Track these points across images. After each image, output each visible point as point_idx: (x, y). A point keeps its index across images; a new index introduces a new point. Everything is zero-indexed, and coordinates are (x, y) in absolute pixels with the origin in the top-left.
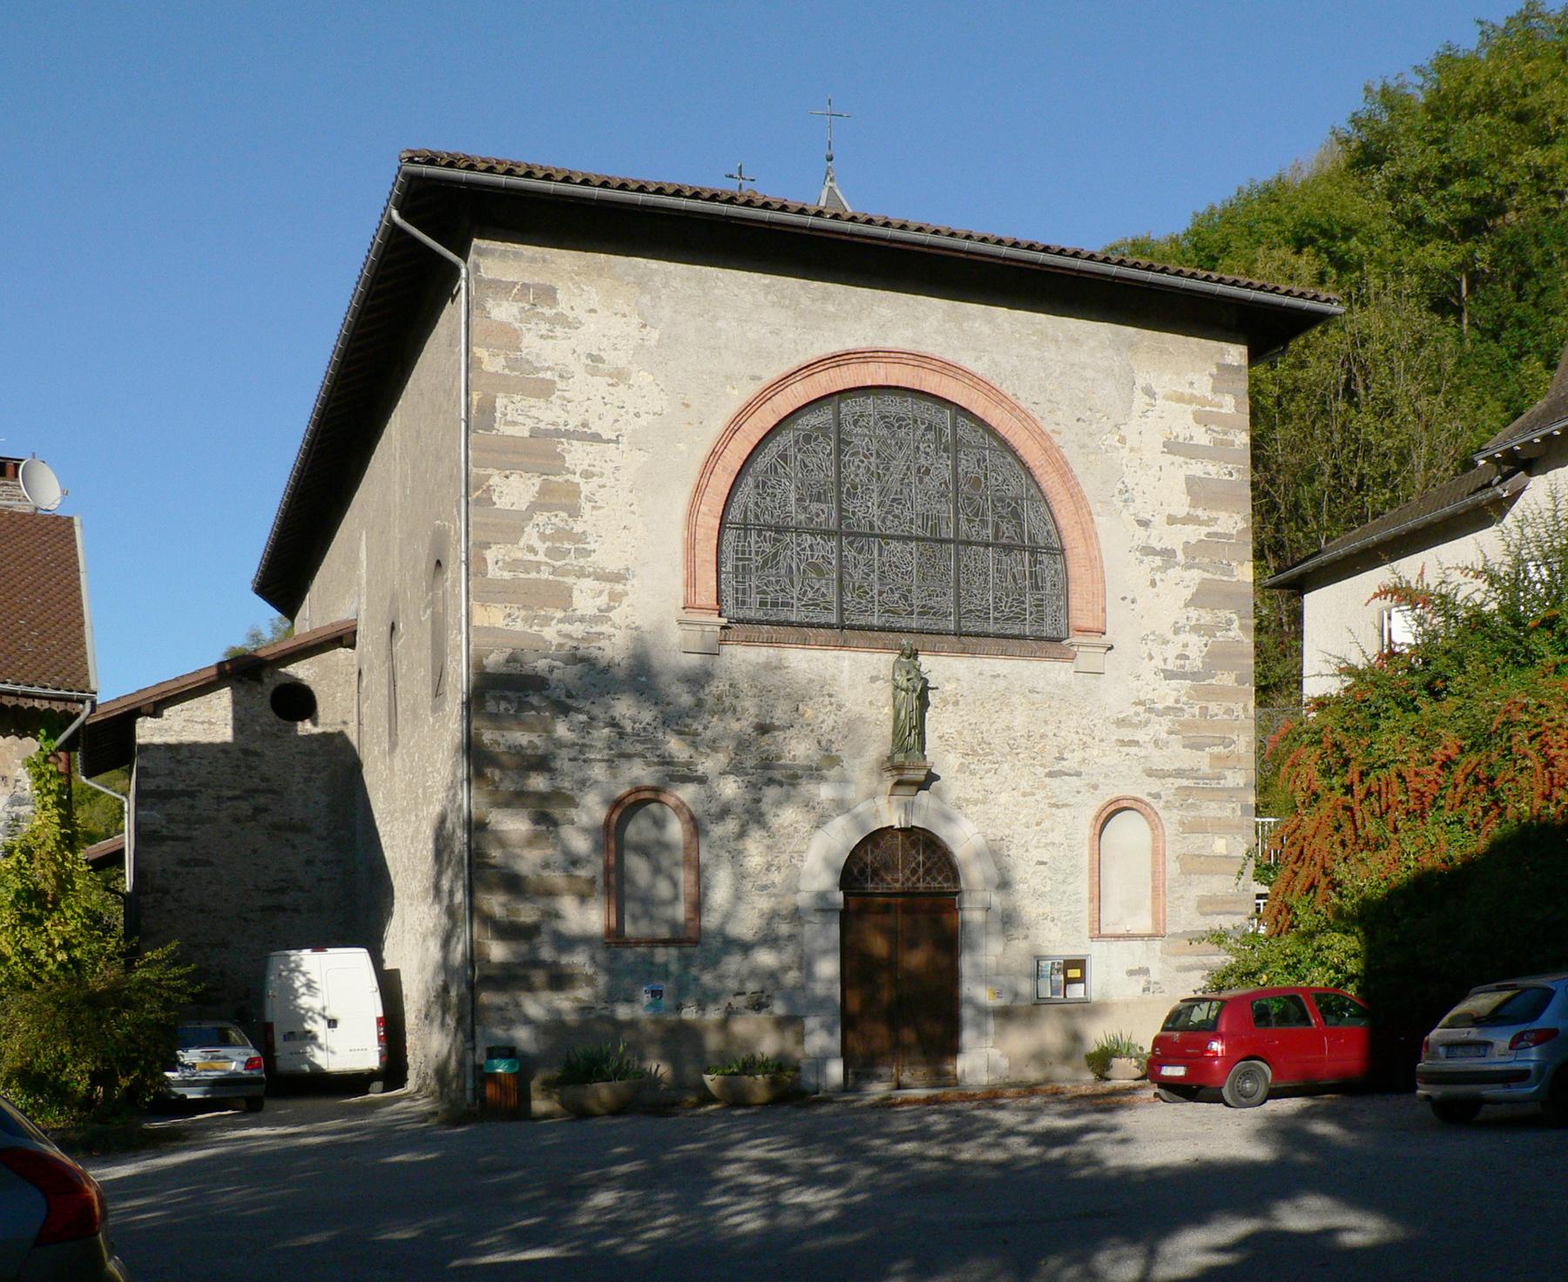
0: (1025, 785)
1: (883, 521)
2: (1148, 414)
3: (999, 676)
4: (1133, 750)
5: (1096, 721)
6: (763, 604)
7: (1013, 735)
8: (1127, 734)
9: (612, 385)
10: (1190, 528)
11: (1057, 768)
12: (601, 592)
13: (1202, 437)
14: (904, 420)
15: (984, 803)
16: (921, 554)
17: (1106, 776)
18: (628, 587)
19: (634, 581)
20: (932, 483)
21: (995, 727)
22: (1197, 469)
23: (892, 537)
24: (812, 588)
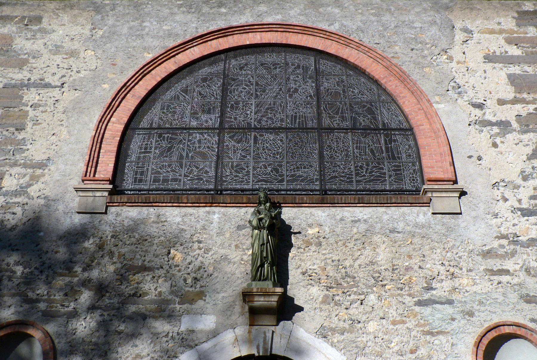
0: (393, 314)
2: (469, 42)
3: (359, 220)
4: (505, 279)
5: (460, 254)
7: (377, 268)
8: (495, 264)
9: (66, 58)
10: (518, 106)
11: (426, 296)
12: (25, 176)
13: (514, 51)
14: (278, 64)
15: (351, 331)
16: (290, 140)
17: (481, 303)
20: (300, 97)
21: (358, 262)
22: (515, 70)
24: (197, 168)
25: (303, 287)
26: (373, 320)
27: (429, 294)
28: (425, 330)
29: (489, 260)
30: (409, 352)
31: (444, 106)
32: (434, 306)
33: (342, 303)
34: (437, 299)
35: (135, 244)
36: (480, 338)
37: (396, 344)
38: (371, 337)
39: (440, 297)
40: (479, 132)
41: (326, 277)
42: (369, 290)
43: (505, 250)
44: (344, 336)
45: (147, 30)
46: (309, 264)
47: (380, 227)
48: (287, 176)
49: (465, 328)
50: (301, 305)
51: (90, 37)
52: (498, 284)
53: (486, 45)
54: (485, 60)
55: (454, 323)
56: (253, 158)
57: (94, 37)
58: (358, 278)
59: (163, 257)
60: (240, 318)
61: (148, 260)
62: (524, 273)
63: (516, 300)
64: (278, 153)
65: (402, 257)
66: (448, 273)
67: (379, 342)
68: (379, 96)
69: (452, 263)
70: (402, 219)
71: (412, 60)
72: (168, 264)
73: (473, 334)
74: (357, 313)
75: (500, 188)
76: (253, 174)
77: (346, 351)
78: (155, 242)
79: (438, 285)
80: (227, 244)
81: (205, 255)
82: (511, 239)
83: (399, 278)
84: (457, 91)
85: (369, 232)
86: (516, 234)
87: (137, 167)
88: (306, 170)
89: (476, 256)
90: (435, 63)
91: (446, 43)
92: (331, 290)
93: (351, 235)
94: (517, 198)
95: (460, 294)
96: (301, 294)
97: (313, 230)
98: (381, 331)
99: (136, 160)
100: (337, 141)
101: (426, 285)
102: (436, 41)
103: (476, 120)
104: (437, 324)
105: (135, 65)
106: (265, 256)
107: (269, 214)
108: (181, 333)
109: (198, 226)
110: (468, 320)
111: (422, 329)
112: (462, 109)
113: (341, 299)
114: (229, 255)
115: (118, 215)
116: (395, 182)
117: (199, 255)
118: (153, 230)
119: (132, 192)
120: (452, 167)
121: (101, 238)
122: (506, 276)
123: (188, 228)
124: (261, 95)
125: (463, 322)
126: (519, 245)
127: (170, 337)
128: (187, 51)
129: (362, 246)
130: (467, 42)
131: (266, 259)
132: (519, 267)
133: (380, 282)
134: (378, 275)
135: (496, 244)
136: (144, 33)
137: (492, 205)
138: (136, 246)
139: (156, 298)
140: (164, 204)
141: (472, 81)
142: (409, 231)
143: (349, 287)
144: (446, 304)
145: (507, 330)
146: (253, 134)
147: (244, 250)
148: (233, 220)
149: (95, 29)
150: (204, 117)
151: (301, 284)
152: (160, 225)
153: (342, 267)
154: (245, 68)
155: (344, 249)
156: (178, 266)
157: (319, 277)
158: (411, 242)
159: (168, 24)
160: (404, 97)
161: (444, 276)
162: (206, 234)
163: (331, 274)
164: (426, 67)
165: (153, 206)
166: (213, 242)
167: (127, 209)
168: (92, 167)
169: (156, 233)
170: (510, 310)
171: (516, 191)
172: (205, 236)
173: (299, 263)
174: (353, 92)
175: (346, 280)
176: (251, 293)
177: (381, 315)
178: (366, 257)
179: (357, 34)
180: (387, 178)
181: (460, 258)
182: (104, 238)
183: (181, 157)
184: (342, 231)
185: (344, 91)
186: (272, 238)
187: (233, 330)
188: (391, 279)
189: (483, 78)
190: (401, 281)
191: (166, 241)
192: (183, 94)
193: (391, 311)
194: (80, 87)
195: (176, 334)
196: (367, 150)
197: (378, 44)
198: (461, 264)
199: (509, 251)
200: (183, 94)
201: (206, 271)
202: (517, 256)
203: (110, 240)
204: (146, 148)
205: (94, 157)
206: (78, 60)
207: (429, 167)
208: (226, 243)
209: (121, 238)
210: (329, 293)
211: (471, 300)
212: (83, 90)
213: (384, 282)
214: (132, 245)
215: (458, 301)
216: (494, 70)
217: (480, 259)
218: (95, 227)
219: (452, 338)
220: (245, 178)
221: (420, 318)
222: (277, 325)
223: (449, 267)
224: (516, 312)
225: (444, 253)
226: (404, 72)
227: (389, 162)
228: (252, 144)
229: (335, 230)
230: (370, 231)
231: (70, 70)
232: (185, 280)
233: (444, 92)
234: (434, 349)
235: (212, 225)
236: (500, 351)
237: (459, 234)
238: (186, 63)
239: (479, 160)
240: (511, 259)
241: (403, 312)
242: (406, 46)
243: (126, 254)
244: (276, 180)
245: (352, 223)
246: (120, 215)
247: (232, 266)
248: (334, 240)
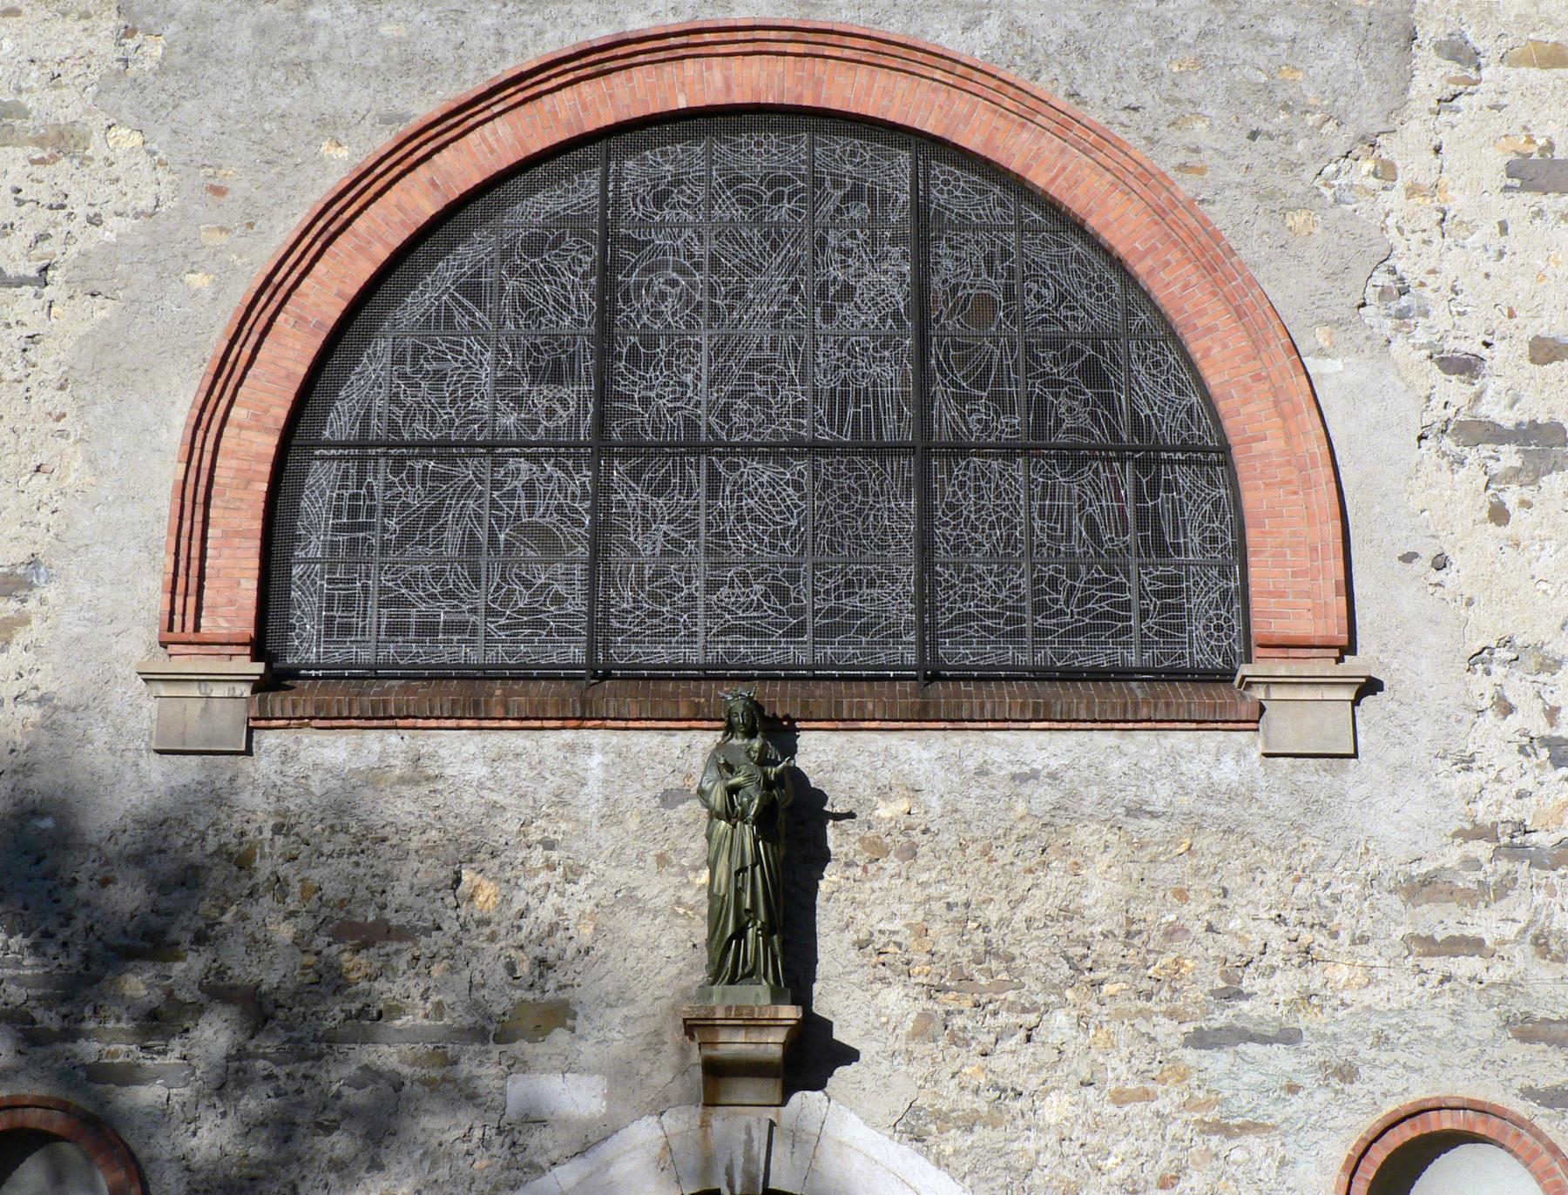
0: (1118, 1071)
1: (724, 415)
2: (1461, 102)
3: (1035, 775)
4: (1466, 966)
5: (1336, 889)
6: (395, 629)
7: (1080, 930)
8: (1441, 920)
9: (42, 161)
11: (1220, 1019)
14: (787, 181)
15: (993, 1122)
16: (827, 485)
17: (1382, 1040)
18: (32, 605)
19: (51, 592)
20: (858, 318)
21: (1025, 910)
23: (749, 450)
24: (528, 585)
25: (860, 987)
26: (1060, 1089)
27: (1229, 1012)
28: (1206, 1119)
29: (1425, 907)
30: (1155, 1184)
31: (1341, 368)
32: (1242, 1047)
33: (973, 1038)
34: (1250, 1027)
35: (350, 854)
36: (1364, 1145)
37: (1119, 1159)
38: (1051, 1139)
39: (1261, 1021)
40: (1452, 464)
41: (929, 956)
42: (1053, 998)
43: (1481, 876)
44: (974, 1137)
45: (322, 38)
46: (877, 916)
47: (1096, 798)
48: (815, 613)
49: (1324, 1114)
50: (852, 1045)
51: (119, 72)
52: (1441, 982)
53: (1524, 117)
54: (1509, 181)
55: (1293, 1100)
56: (708, 552)
57: (133, 68)
58: (1023, 960)
59: (441, 895)
60: (677, 1083)
61: (394, 906)
62: (1529, 949)
63: (1489, 1033)
64: (785, 531)
65: (1157, 896)
66: (1294, 947)
67: (1071, 1152)
68: (1129, 314)
69: (1308, 917)
70: (1166, 770)
71: (1249, 179)
72: (458, 917)
73: (1346, 1133)
74: (1015, 1066)
75: (1494, 667)
76: (708, 607)
77: (976, 1181)
78: (414, 845)
79: (1260, 984)
80: (631, 853)
81: (567, 886)
82: (1505, 840)
83: (1145, 960)
84: (1395, 306)
85: (1062, 814)
86: (1522, 823)
87: (330, 581)
88: (875, 592)
89: (1385, 894)
90: (1328, 193)
91: (1377, 106)
92: (940, 996)
93: (1008, 825)
94: (1545, 703)
95: (1321, 1012)
96: (852, 1009)
97: (892, 806)
98: (1080, 1122)
99: (323, 552)
100: (978, 489)
101: (1222, 985)
102: (1342, 100)
103: (1448, 421)
104: (1244, 1103)
105: (292, 193)
106: (748, 906)
107: (759, 776)
108: (508, 1128)
109: (544, 794)
110: (1337, 1092)
111: (1198, 1116)
112: (1403, 379)
113: (970, 1025)
115: (287, 757)
116: (1158, 633)
117: (548, 886)
118: (401, 808)
119: (320, 673)
120: (1343, 600)
121: (243, 834)
122: (1472, 959)
123: (513, 800)
124: (731, 308)
125: (1320, 1096)
126: (1528, 862)
127: (475, 1140)
128: (471, 136)
129: (1038, 858)
130: (1455, 102)
131: (752, 915)
132: (1516, 930)
133: (1086, 973)
134: (1081, 950)
135: (1453, 856)
136: (313, 52)
137: (1457, 727)
138: (354, 858)
139: (426, 1022)
140: (433, 723)
141: (1451, 268)
142: (1185, 810)
143: (994, 989)
144: (1277, 1041)
145: (1447, 1122)
146: (703, 460)
147: (683, 872)
148: (648, 771)
149: (134, 31)
150: (542, 396)
151: (854, 978)
152: (424, 789)
153: (975, 925)
154: (675, 197)
155: (985, 868)
156: (488, 923)
157: (907, 956)
158: (1189, 849)
159: (398, 14)
160: (1210, 330)
161: (1281, 956)
162: (569, 820)
163: (942, 948)
164: (1294, 209)
165: (396, 728)
166: (590, 845)
167: (315, 738)
168: (186, 596)
169: (412, 818)
170: (1465, 1062)
171: (1544, 677)
172: (563, 826)
173: (849, 912)
174: (1039, 296)
175: (985, 965)
177: (1083, 1074)
178: (1049, 894)
179: (1063, 66)
180: (1132, 623)
181: (1336, 899)
182: (251, 835)
183: (472, 545)
184: (981, 808)
185: (1009, 293)
186: (769, 845)
187: (656, 1118)
188: (1121, 965)
189: (1493, 253)
190: (1150, 972)
191: (445, 842)
192: (466, 302)
193: (1114, 1062)
194: (109, 283)
195: (494, 1131)
196: (1076, 521)
197: (1136, 109)
198: (1336, 921)
199: (1491, 880)
200: (466, 302)
201: (571, 938)
202: (1513, 894)
203: (272, 839)
204: (354, 511)
205: (189, 558)
206: (86, 170)
207: (1270, 594)
208: (628, 851)
209: (305, 835)
210: (936, 1007)
211: (1354, 1033)
212: (121, 295)
213: (1099, 975)
214: (340, 855)
215: (1312, 1035)
216: (1538, 221)
217: (1398, 906)
218: (219, 796)
219: (1282, 1145)
221: (1195, 1083)
222: (784, 1103)
223: (1298, 928)
224: (1484, 1068)
225: (1287, 884)
226: (1216, 236)
227: (1144, 566)
228: (703, 501)
229: (960, 806)
230: (1066, 809)
231: (63, 212)
232: (511, 968)
233: (1347, 313)
234: (1228, 1175)
235: (586, 790)
236: (1426, 1175)
237: (1340, 824)
238: (471, 186)
239: (1438, 569)
240: (1494, 906)
241: (1146, 1067)
242: (1233, 118)
243: (324, 887)
244: (779, 626)
245: (1012, 784)
246: (295, 757)
247: (649, 921)
248: (954, 838)
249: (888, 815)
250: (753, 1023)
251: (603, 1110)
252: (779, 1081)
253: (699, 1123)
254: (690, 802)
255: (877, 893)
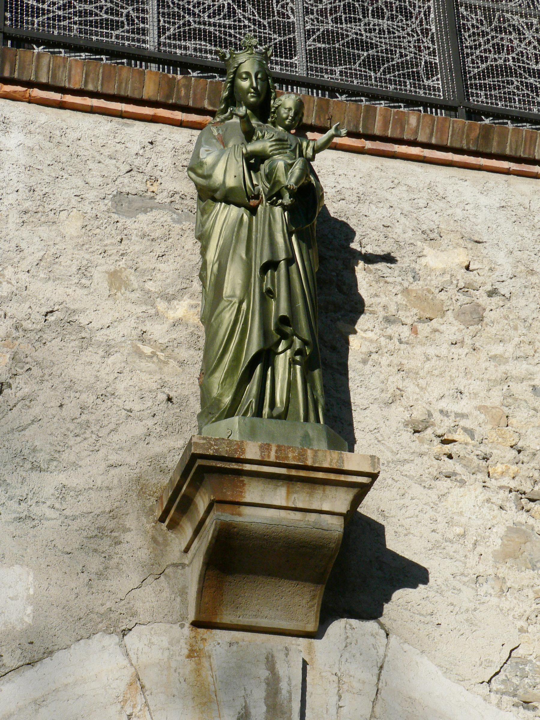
41: (515, 452)
48: (308, 34)
50: (415, 559)
88: (385, 23)
96: (410, 512)
114: (83, 311)
173: (395, 381)
176: (234, 466)
186: (304, 246)
187: (115, 639)
220: (125, 12)
249: (441, 266)
250: (302, 473)
251: (28, 620)
252: (320, 590)
253: (186, 652)
254: (155, 213)
255: (434, 362)
